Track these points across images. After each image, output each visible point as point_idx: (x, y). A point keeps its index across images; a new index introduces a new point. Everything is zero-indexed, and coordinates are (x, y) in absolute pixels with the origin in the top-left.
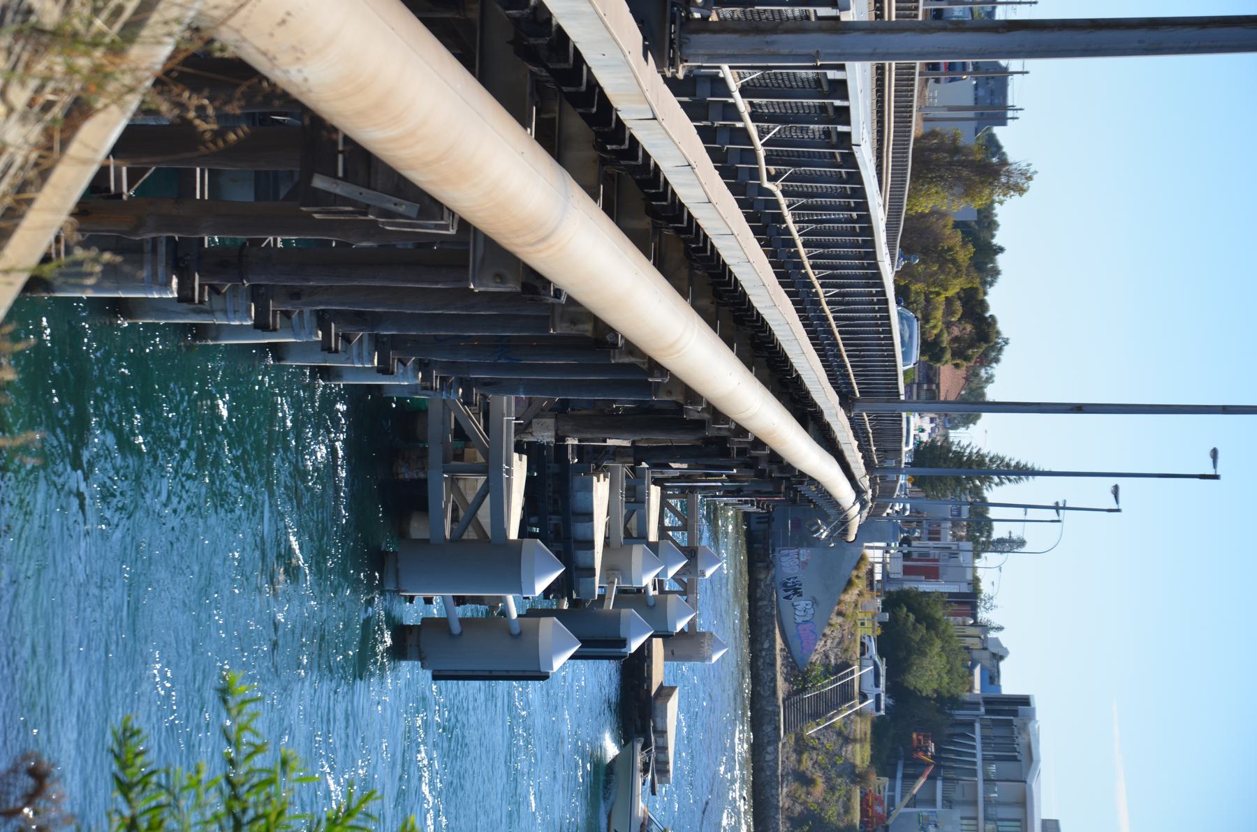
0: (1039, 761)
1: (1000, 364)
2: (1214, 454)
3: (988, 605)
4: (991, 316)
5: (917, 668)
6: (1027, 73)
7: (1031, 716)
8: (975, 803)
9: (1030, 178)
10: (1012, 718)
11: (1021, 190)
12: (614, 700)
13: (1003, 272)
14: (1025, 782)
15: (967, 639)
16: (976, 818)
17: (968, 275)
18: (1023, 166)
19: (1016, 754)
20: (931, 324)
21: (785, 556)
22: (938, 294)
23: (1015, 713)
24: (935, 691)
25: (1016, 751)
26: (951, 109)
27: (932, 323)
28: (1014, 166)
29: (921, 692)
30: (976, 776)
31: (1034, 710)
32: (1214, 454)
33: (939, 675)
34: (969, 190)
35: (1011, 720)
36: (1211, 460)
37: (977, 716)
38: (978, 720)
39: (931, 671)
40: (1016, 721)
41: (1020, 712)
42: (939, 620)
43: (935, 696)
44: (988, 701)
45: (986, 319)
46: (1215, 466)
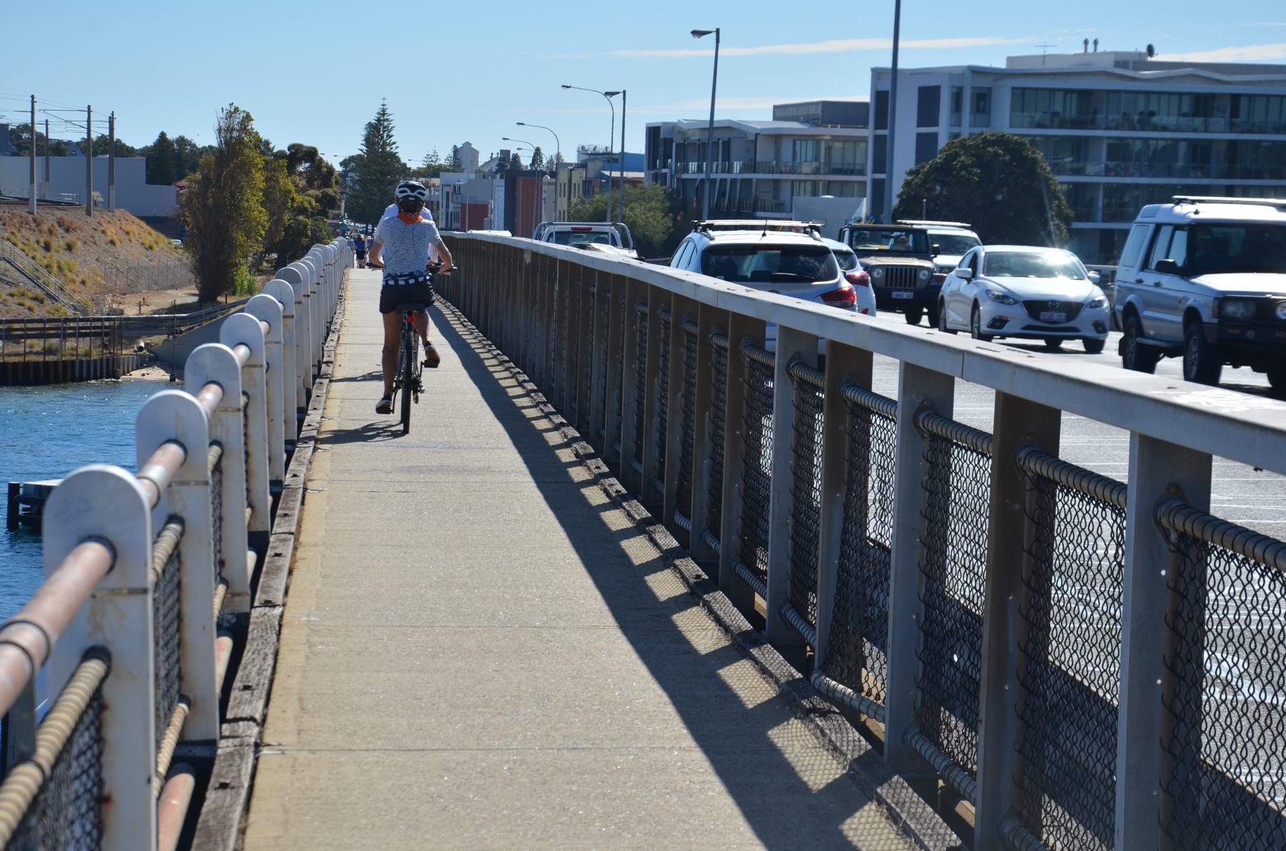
0: (730, 121)
1: (271, 141)
2: (697, 33)
3: (434, 159)
4: (289, 149)
5: (647, 231)
6: (89, 107)
7: (673, 127)
8: (776, 182)
9: (237, 109)
10: (674, 145)
11: (248, 118)
12: (1032, 261)
13: (181, 134)
14: (757, 135)
15: (574, 181)
16: (793, 181)
17: (275, 170)
18: (222, 115)
19: (720, 142)
20: (308, 206)
21: (387, 397)
22: (293, 200)
23: (668, 142)
24: (666, 214)
25: (718, 143)
26: (32, 181)
27: (306, 205)
28: (222, 122)
29: (669, 228)
30: (751, 180)
31: (664, 123)
32: (697, 33)
33: (649, 210)
34: (246, 168)
35: (677, 145)
36: (703, 37)
37: (672, 176)
38: (678, 176)
39: (647, 218)
40: (677, 139)
41: (667, 136)
42: (596, 209)
43: (671, 214)
44: (652, 165)
45: (291, 154)
46: (710, 32)
